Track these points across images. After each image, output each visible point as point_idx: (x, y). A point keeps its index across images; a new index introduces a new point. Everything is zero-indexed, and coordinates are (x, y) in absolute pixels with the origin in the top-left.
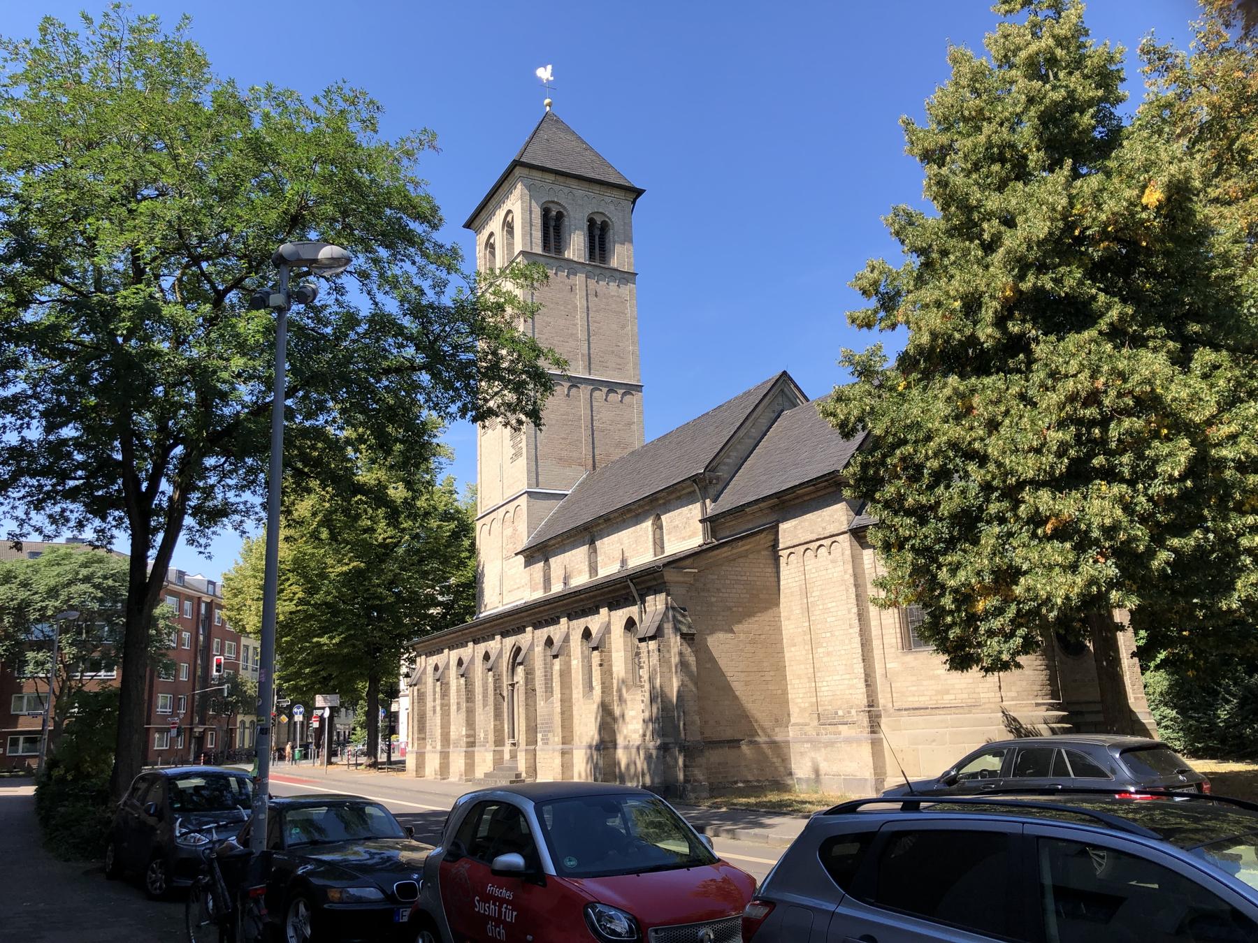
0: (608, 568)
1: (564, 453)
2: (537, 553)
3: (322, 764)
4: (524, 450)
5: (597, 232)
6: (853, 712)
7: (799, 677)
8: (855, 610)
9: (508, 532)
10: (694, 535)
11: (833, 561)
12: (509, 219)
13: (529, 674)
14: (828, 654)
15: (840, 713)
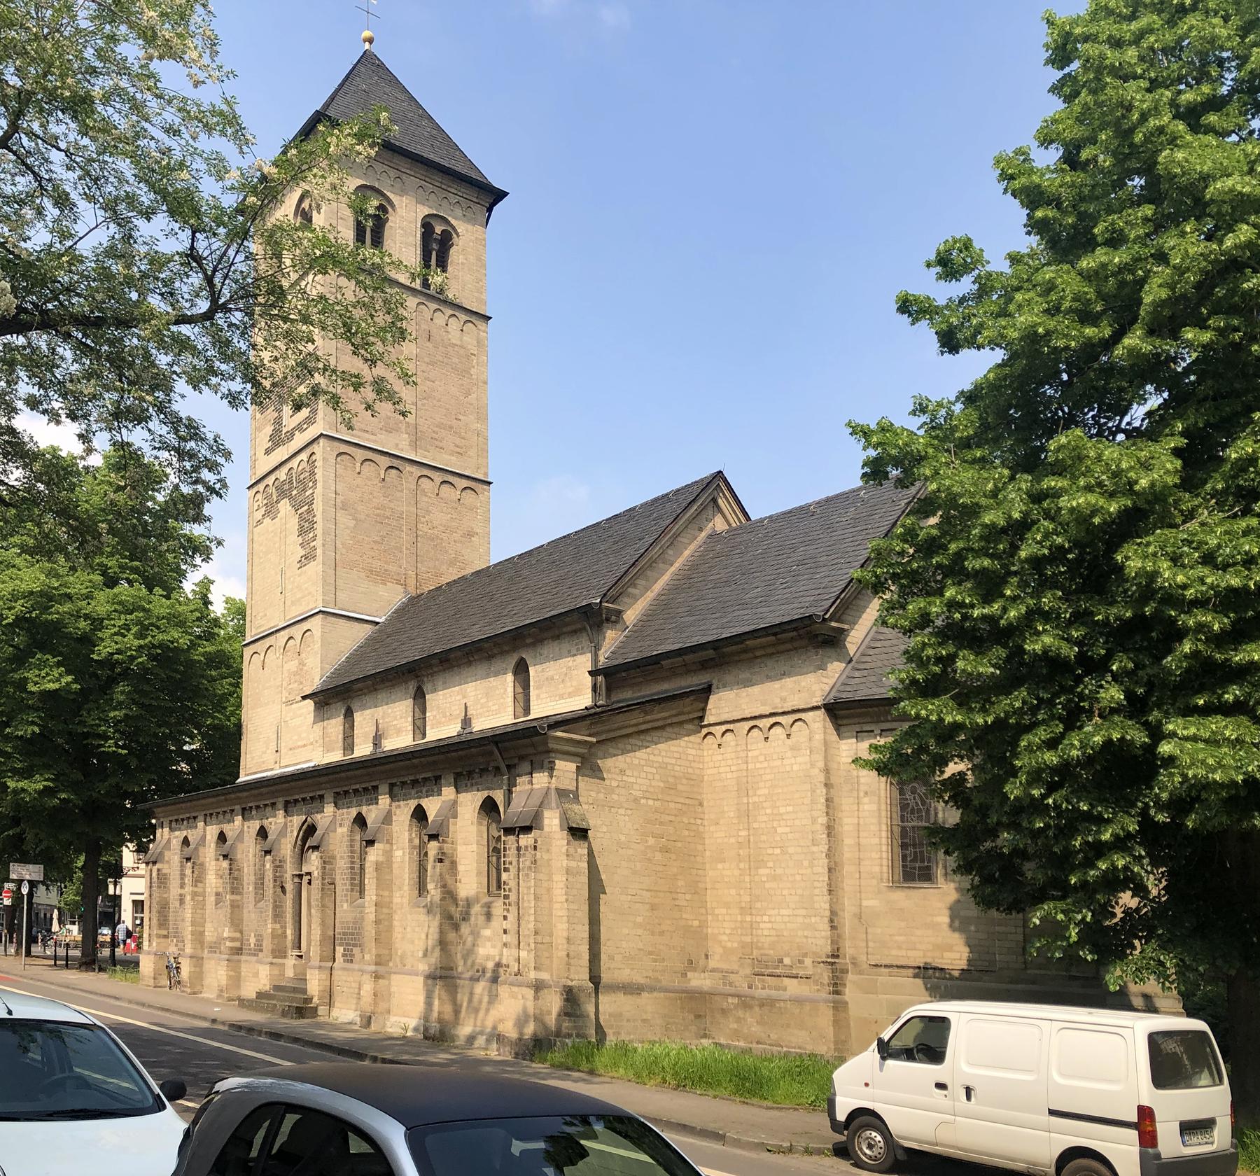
0: (442, 728)
1: (376, 564)
2: (337, 696)
3: (17, 953)
6: (808, 961)
7: (727, 906)
8: (823, 820)
9: (292, 665)
10: (577, 692)
11: (793, 748)
12: (305, 205)
13: (326, 862)
14: (775, 878)
15: (787, 961)
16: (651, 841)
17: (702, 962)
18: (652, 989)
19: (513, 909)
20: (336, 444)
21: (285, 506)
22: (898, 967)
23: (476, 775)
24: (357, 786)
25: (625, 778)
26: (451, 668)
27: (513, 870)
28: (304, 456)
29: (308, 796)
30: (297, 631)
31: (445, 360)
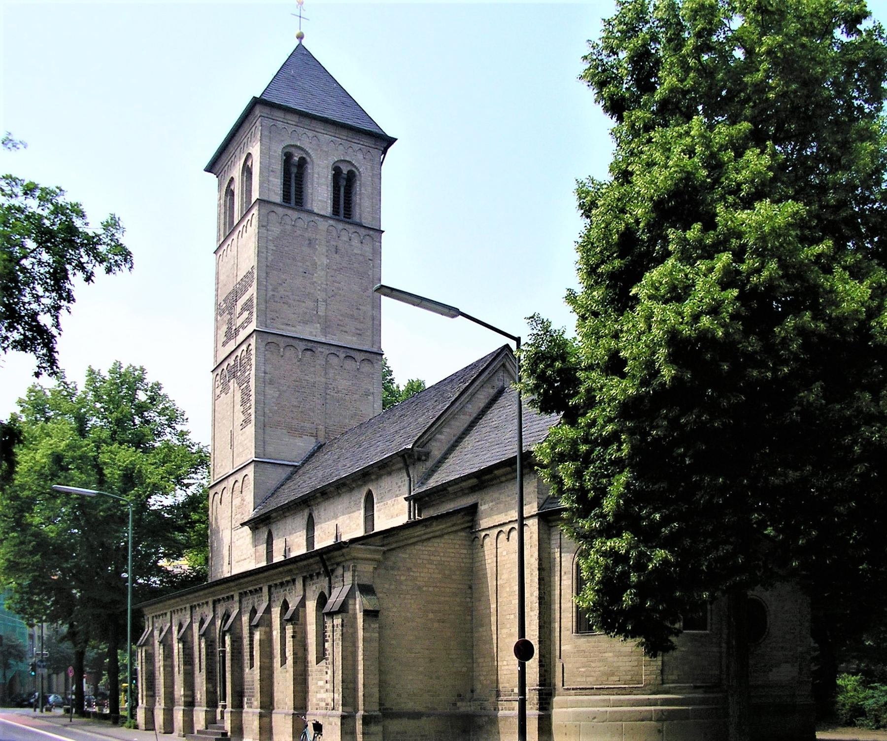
0: (324, 539)
4: (253, 417)
5: (343, 183)
16: (431, 616)
17: (468, 696)
18: (429, 716)
19: (330, 666)
20: (266, 336)
21: (233, 384)
22: (580, 689)
23: (315, 578)
24: (250, 588)
25: (412, 574)
26: (328, 498)
27: (330, 639)
28: (244, 347)
29: (225, 596)
30: (239, 477)
31: (349, 266)
